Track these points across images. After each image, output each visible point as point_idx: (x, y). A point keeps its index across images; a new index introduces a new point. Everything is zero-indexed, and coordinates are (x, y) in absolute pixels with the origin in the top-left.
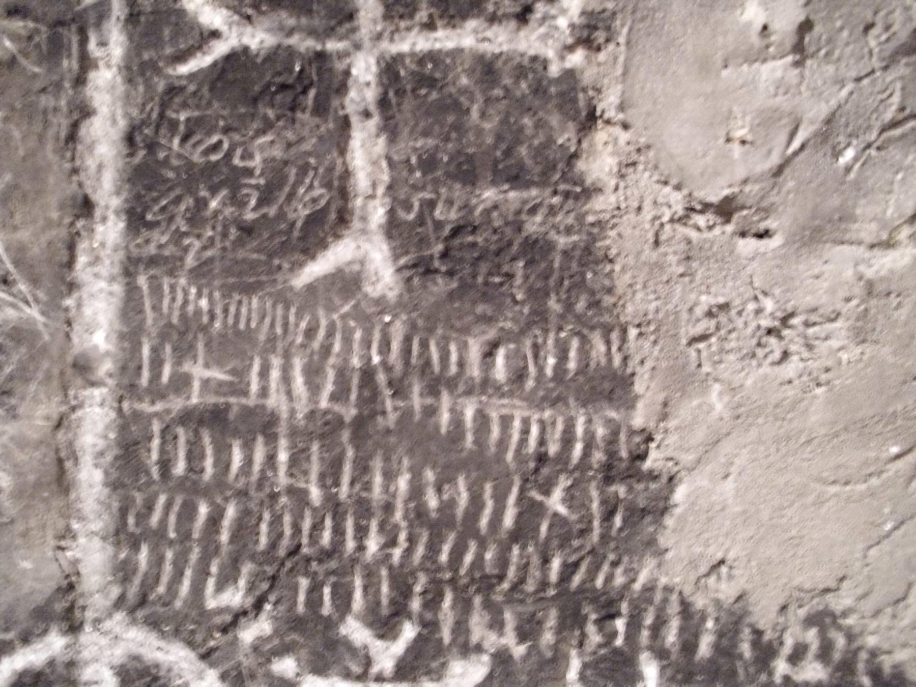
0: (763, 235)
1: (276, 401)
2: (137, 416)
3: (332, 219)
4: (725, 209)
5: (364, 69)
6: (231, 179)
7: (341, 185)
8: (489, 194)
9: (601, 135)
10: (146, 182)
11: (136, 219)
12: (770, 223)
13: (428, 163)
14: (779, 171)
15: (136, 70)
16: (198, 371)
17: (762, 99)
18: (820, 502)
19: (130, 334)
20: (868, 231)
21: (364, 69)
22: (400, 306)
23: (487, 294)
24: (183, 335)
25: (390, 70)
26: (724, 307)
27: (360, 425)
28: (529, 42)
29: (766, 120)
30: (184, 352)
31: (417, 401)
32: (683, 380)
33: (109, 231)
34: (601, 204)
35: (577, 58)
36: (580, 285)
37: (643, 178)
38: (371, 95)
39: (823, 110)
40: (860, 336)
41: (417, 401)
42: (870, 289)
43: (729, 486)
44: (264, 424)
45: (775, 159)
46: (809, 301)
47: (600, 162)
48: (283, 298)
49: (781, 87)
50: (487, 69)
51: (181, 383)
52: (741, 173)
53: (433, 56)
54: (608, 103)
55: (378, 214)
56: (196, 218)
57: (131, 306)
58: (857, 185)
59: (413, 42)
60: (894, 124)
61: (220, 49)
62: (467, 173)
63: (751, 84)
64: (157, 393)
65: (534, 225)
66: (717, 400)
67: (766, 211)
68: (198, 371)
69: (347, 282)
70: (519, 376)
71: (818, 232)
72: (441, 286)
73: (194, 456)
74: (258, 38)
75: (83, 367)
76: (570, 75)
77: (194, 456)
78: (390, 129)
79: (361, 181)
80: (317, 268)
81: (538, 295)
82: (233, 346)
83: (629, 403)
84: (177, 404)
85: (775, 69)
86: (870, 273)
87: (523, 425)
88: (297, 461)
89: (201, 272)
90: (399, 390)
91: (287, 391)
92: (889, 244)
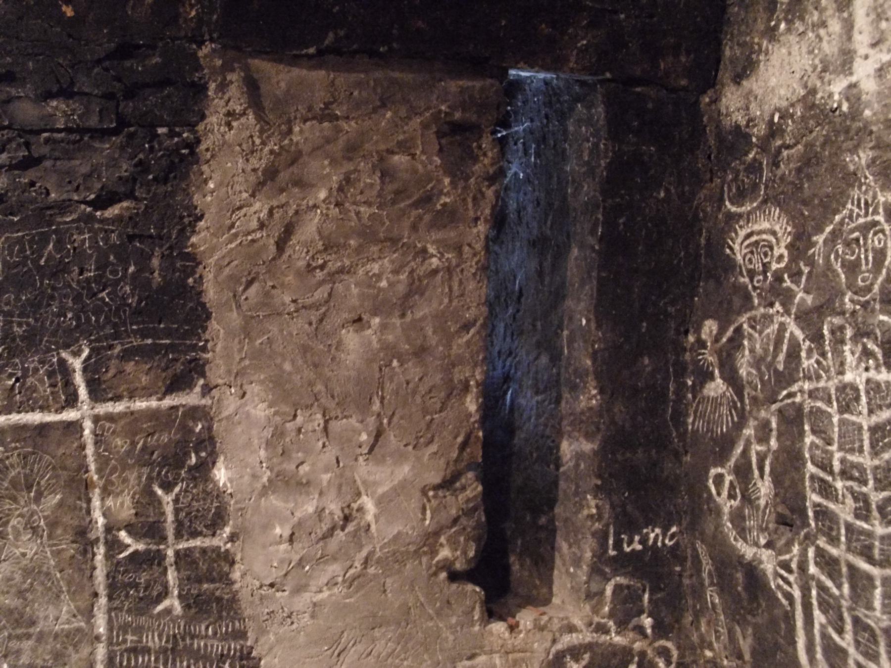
0: (284, 591)
1: (150, 644)
2: (113, 651)
3: (165, 593)
4: (272, 585)
5: (170, 553)
6: (136, 586)
7: (166, 586)
8: (206, 586)
9: (237, 566)
10: (113, 588)
11: (110, 598)
12: (285, 588)
13: (189, 579)
14: (286, 575)
15: (108, 557)
16: (130, 637)
17: (281, 555)
18: (304, 663)
19: (110, 629)
20: (314, 589)
21: (170, 553)
22: (183, 617)
23: (206, 612)
24: (125, 628)
25: (177, 553)
26: (273, 612)
27: (173, 649)
28: (216, 542)
29: (282, 561)
30: (125, 633)
31: (188, 641)
32: (263, 631)
33: (103, 600)
34: (236, 586)
35: (229, 545)
36: (232, 608)
37: (248, 578)
38: (173, 560)
39: (298, 557)
40: (313, 617)
41: (188, 641)
42: (315, 604)
43: (276, 660)
44: (147, 651)
45: (284, 572)
46: (297, 609)
47: (236, 575)
48: (151, 617)
49: (286, 551)
50: (204, 551)
51: (125, 641)
52: (275, 576)
53: (189, 549)
54: (238, 558)
55: (176, 592)
56: (127, 596)
57: (110, 621)
58: (310, 576)
59: (183, 545)
60: (320, 558)
61: (131, 550)
62: (199, 581)
63: (278, 551)
64: (118, 644)
65: (218, 593)
66: (272, 637)
67: (284, 585)
68: (130, 637)
69: (168, 611)
70: (215, 633)
71: (299, 590)
72: (193, 611)
73: (129, 660)
74: (141, 547)
75: (98, 638)
76: (227, 551)
77: (129, 660)
78: (178, 569)
79: (171, 583)
80: (160, 608)
81: (220, 612)
82: (139, 630)
83: (247, 639)
84: (124, 647)
85: (284, 546)
86: (314, 600)
87: (217, 647)
88: (157, 660)
89: (129, 611)
90: (183, 639)
91: (153, 641)
92: (321, 591)
